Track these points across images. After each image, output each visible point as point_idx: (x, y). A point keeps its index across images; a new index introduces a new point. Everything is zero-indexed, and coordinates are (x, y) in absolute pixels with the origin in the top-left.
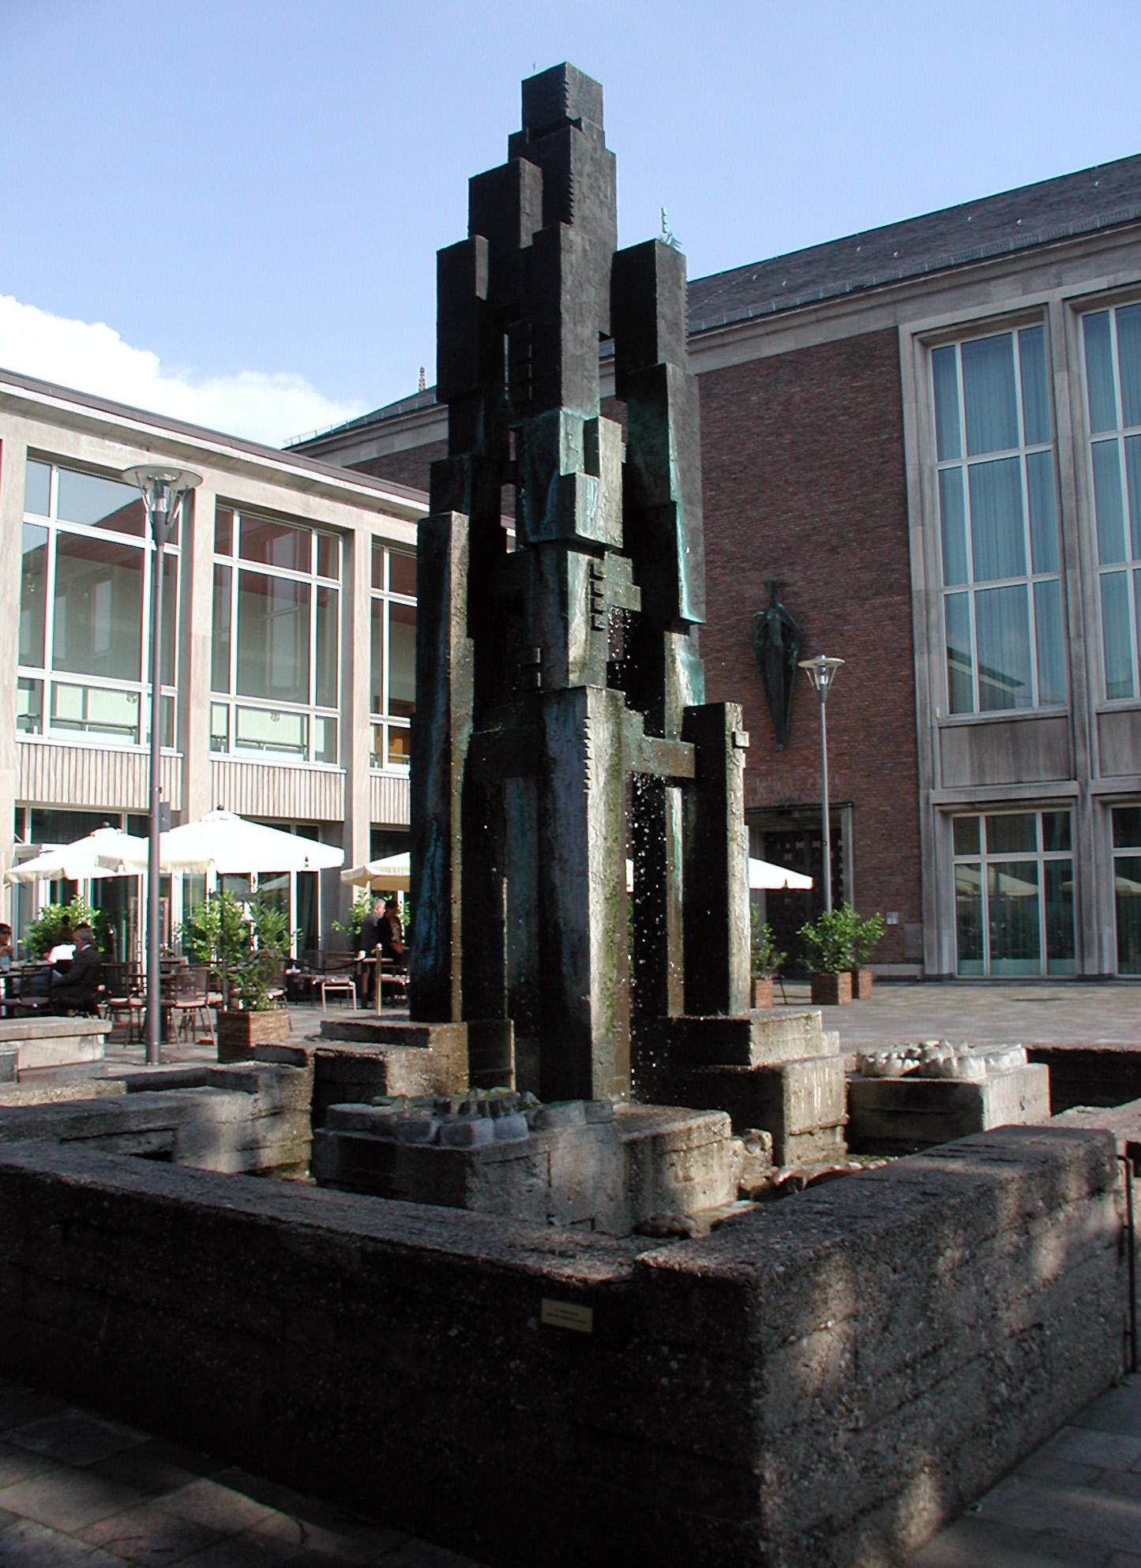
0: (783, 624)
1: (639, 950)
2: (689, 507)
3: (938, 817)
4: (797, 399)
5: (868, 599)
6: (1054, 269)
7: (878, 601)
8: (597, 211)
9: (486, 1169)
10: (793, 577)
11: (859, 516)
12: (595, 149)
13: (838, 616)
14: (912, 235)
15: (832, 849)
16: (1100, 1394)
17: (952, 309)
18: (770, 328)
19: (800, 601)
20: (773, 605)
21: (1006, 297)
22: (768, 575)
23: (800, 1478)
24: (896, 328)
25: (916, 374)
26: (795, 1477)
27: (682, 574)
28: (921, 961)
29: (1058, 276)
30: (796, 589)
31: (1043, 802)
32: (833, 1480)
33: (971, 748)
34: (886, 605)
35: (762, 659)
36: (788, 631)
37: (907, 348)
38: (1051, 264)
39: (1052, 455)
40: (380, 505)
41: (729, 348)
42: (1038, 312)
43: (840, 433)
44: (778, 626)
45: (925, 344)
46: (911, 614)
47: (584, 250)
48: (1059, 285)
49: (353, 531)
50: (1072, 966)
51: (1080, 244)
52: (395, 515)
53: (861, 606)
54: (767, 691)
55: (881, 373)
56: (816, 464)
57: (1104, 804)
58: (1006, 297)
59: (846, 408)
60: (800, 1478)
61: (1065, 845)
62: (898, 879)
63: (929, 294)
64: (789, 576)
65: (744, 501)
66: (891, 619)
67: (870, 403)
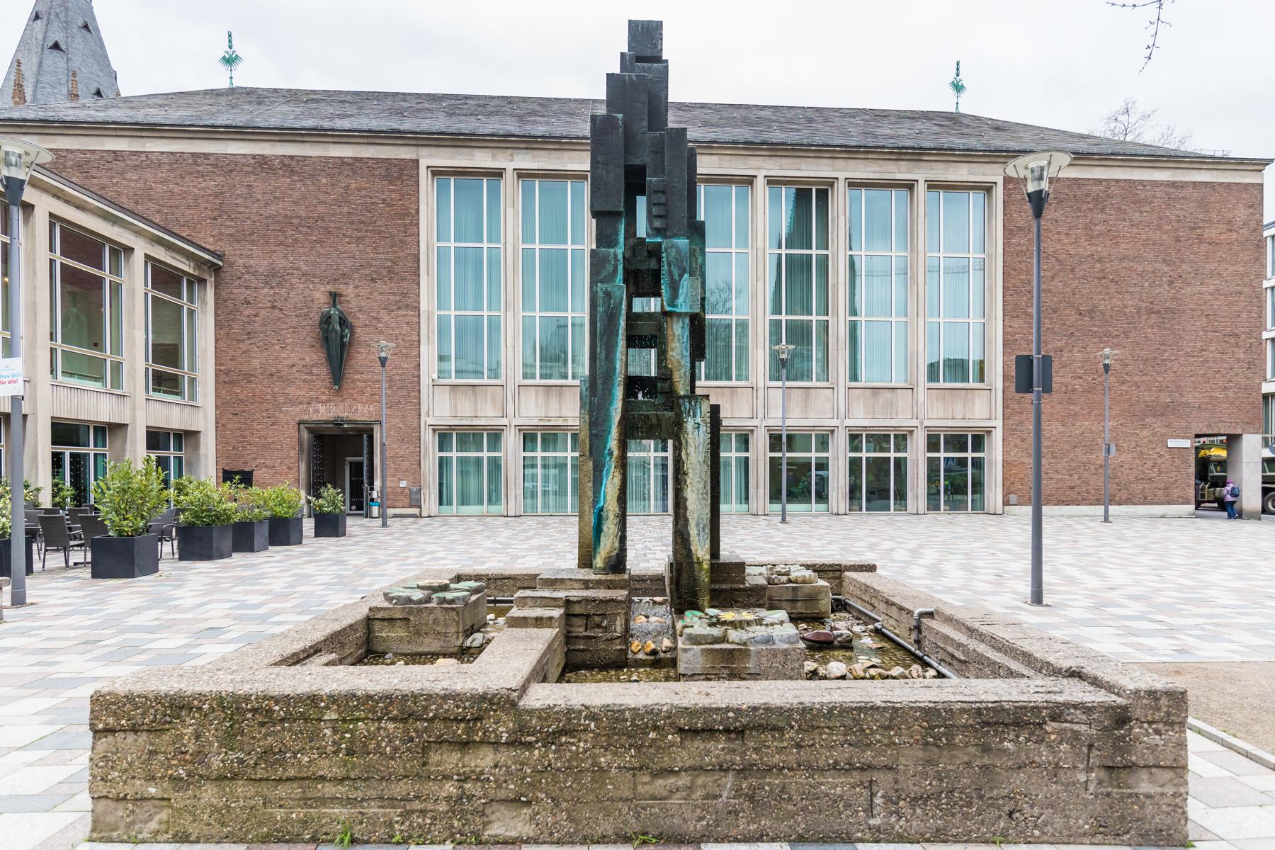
1: (712, 449)
6: (510, 151)
7: (400, 313)
10: (348, 291)
11: (389, 264)
15: (607, 419)
16: (689, 730)
17: (452, 158)
20: (335, 306)
21: (481, 159)
22: (330, 288)
25: (427, 188)
28: (420, 507)
29: (512, 156)
36: (343, 322)
37: (424, 175)
40: (55, 192)
49: (33, 206)
50: (494, 509)
52: (66, 202)
58: (481, 159)
59: (384, 200)
61: (441, 459)
64: (341, 288)
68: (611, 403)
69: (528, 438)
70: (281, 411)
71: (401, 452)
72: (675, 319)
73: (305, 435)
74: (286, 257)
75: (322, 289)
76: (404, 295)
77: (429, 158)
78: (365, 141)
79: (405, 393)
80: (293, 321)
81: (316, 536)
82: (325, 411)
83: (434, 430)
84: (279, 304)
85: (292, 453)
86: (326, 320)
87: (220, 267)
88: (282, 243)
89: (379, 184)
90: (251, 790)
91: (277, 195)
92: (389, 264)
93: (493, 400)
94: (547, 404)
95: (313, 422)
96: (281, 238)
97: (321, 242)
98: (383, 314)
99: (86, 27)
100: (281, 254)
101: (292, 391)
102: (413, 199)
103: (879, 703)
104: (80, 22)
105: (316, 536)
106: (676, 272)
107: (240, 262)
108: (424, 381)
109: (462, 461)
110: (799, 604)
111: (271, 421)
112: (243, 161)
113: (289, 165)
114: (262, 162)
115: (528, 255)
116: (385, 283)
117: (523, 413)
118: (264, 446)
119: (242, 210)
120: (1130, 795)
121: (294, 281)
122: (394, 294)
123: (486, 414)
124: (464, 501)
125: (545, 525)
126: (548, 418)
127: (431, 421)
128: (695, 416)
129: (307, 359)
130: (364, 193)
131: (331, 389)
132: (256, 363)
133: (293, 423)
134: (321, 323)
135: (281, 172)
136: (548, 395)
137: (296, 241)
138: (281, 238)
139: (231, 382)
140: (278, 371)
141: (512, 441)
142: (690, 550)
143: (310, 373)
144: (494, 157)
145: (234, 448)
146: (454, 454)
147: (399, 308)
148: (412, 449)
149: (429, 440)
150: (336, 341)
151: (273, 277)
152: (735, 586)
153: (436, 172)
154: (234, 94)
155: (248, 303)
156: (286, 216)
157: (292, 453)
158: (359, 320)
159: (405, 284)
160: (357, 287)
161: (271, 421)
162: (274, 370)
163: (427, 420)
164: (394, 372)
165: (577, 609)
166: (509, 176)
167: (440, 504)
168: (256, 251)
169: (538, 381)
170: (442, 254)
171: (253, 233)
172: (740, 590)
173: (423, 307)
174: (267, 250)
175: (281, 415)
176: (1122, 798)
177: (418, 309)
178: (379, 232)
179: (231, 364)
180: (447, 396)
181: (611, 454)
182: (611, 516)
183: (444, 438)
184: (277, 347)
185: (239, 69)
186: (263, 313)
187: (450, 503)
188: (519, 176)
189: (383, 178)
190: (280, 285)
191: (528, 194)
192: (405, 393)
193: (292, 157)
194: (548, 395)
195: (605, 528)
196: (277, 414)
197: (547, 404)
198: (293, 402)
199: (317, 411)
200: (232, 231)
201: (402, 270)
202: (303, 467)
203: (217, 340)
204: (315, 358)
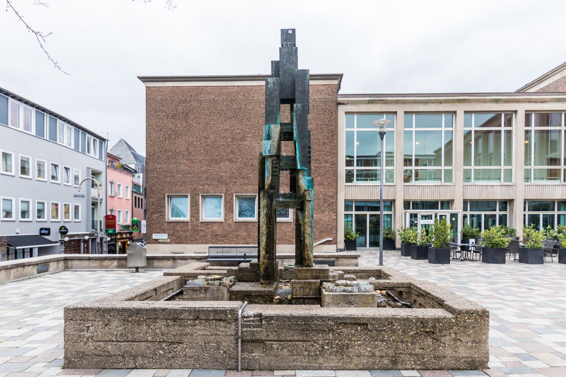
27: (297, 159)
47: (274, 82)
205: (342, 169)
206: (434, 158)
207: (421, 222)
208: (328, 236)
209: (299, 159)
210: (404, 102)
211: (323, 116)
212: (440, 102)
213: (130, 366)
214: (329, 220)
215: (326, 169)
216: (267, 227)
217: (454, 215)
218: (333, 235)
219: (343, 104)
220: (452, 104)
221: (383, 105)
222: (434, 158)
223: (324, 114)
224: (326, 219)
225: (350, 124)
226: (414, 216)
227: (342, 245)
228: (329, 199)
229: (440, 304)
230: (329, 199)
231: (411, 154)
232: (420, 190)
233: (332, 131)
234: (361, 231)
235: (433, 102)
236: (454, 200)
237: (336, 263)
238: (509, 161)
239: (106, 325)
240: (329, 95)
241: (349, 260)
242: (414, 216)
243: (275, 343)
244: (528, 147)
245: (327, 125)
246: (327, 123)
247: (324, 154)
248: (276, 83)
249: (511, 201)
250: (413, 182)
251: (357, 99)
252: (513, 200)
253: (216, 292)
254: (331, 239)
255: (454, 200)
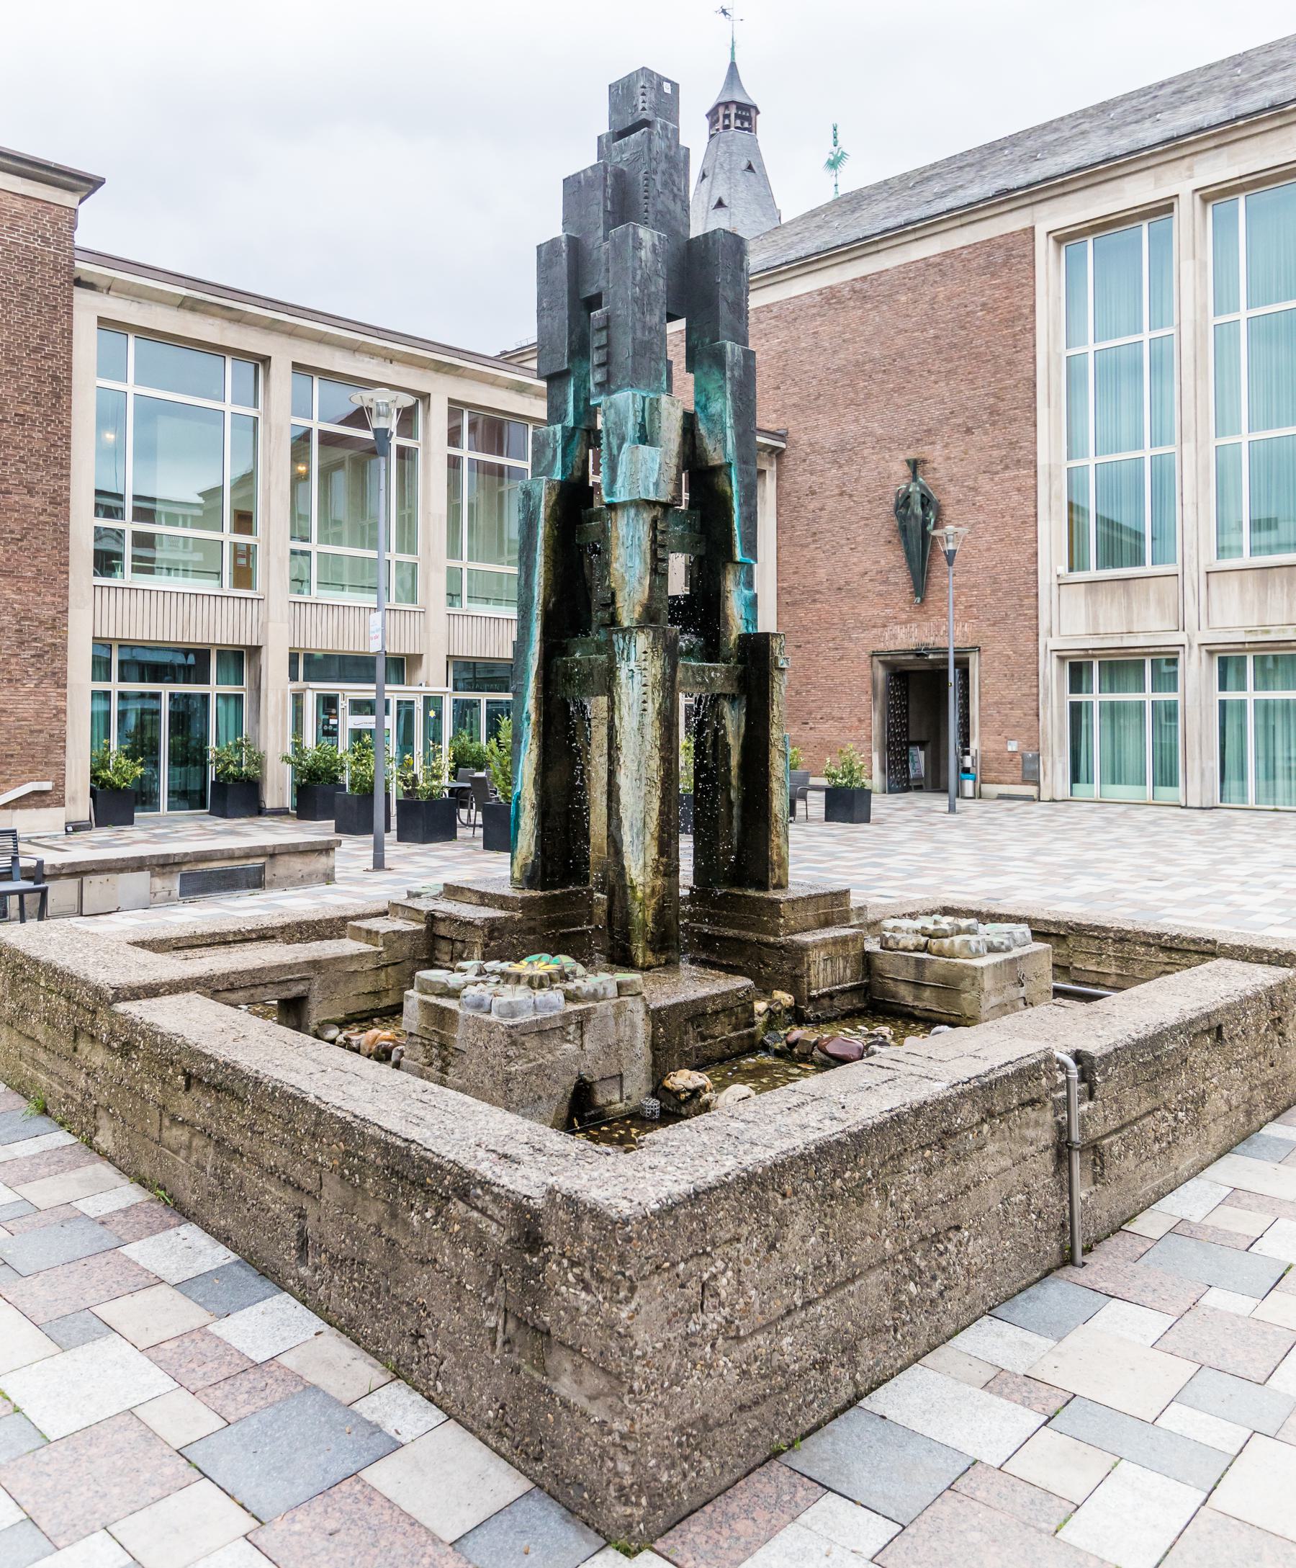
0: (923, 496)
2: (743, 466)
3: (1055, 661)
4: (941, 296)
5: (997, 473)
7: (1008, 474)
8: (671, 206)
9: (523, 1038)
10: (935, 453)
11: (992, 400)
12: (669, 147)
13: (971, 489)
14: (1055, 136)
18: (918, 235)
19: (937, 475)
20: (915, 479)
21: (1137, 191)
22: (911, 454)
23: (671, 1386)
24: (1033, 228)
25: (1048, 265)
26: (666, 1384)
27: (735, 526)
28: (1038, 783)
29: (1190, 168)
30: (935, 465)
31: (1152, 650)
32: (708, 1385)
33: (1087, 605)
34: (1014, 478)
35: (903, 530)
36: (926, 501)
38: (1183, 157)
39: (1176, 338)
41: (882, 254)
42: (1165, 208)
43: (978, 327)
44: (918, 497)
45: (1059, 241)
46: (1036, 486)
47: (654, 245)
48: (1191, 177)
50: (1166, 793)
51: (1214, 136)
53: (992, 479)
54: (908, 552)
55: (1018, 271)
56: (956, 356)
57: (1211, 653)
58: (1137, 191)
59: (984, 305)
60: (671, 1386)
62: (1018, 712)
63: (1064, 194)
65: (893, 390)
66: (1019, 490)
67: (1007, 298)
68: (529, 646)
69: (1228, 665)
70: (851, 639)
71: (1010, 694)
72: (619, 513)
73: (881, 673)
74: (856, 420)
75: (902, 457)
76: (1013, 445)
77: (1052, 217)
78: (958, 222)
79: (1015, 601)
80: (864, 510)
81: (827, 819)
82: (905, 636)
83: (1061, 659)
84: (847, 489)
85: (864, 698)
86: (904, 501)
87: (783, 450)
88: (852, 402)
89: (976, 282)
90: (16, 1039)
91: (847, 336)
92: (992, 400)
93: (1160, 602)
94: (1263, 603)
95: (889, 653)
96: (851, 395)
97: (899, 390)
98: (983, 481)
99: (750, 168)
100: (850, 417)
101: (867, 611)
102: (1027, 291)
103: (311, 1099)
104: (744, 165)
105: (827, 819)
106: (614, 442)
107: (805, 438)
108: (1045, 579)
109: (1266, 709)
110: (927, 993)
111: (837, 654)
112: (808, 301)
113: (860, 292)
114: (830, 297)
115: (1225, 334)
116: (986, 433)
117: (1217, 621)
118: (830, 689)
119: (807, 367)
120: (542, 1388)
121: (866, 452)
122: (998, 447)
123: (1146, 626)
124: (1116, 775)
125: (1227, 824)
126: (1265, 629)
127: (1055, 643)
128: (629, 659)
129: (883, 562)
130: (956, 301)
131: (911, 602)
132: (822, 574)
133: (865, 656)
134: (897, 508)
135: (851, 303)
136: (1264, 585)
137: (868, 396)
138: (851, 395)
139: (794, 604)
140: (847, 583)
141: (1196, 675)
142: (623, 868)
143: (886, 582)
144: (1158, 179)
145: (798, 693)
146: (1095, 697)
147: (1007, 467)
148: (1026, 690)
149: (1053, 677)
150: (916, 530)
151: (844, 452)
152: (752, 936)
153: (1063, 238)
154: (853, 202)
155: (813, 493)
156: (857, 364)
157: (864, 698)
158: (949, 496)
159: (1014, 428)
160: (946, 446)
161: (837, 654)
162: (842, 582)
163: (1049, 642)
164: (1000, 568)
165: (442, 930)
166: (1186, 209)
167: (1075, 778)
168: (823, 420)
169: (1247, 560)
170: (1074, 370)
171: (820, 395)
172: (767, 945)
173: (1042, 460)
174: (835, 415)
175: (851, 645)
176: (530, 1386)
177: (1034, 463)
178: (978, 356)
179: (795, 580)
180: (1081, 601)
181: (528, 718)
182: (528, 807)
183: (1078, 672)
184: (846, 549)
185: (845, 168)
186: (830, 504)
187: (1089, 781)
188: (1205, 200)
189: (983, 270)
190: (850, 461)
191: (1224, 229)
192: (1015, 601)
193: (864, 278)
194: (1264, 585)
195: (522, 823)
196: (846, 644)
197: (1263, 603)
198: (865, 626)
199: (895, 637)
200: (795, 400)
201: (1011, 408)
202: (876, 718)
203: (778, 548)
204: (892, 558)
205: (84, 524)
206: (198, 512)
207: (348, 722)
208: (32, 774)
209: (739, 527)
210: (293, 333)
211: (17, 315)
212: (391, 358)
213: (846, 1392)
214: (38, 714)
215: (30, 518)
216: (662, 758)
217: (432, 702)
218: (53, 771)
219: (91, 286)
220: (419, 372)
221: (226, 324)
222: (198, 512)
223: (20, 304)
224: (27, 707)
225: (110, 366)
226: (328, 704)
227: (82, 808)
228: (40, 632)
229: (1205, 950)
230: (40, 632)
231: (121, 492)
232: (332, 620)
233: (55, 378)
234: (142, 747)
235: (373, 353)
236: (419, 657)
237: (268, 876)
238: (408, 541)
239: (772, 1247)
240: (45, 240)
241: (307, 859)
242: (328, 704)
243: (1114, 1138)
244: (454, 510)
245: (35, 350)
246: (35, 342)
247: (22, 460)
248: (659, 250)
249: (255, 650)
250: (127, 577)
251: (136, 279)
252: (260, 647)
253: (612, 1023)
254: (47, 786)
255: (419, 657)
